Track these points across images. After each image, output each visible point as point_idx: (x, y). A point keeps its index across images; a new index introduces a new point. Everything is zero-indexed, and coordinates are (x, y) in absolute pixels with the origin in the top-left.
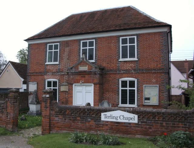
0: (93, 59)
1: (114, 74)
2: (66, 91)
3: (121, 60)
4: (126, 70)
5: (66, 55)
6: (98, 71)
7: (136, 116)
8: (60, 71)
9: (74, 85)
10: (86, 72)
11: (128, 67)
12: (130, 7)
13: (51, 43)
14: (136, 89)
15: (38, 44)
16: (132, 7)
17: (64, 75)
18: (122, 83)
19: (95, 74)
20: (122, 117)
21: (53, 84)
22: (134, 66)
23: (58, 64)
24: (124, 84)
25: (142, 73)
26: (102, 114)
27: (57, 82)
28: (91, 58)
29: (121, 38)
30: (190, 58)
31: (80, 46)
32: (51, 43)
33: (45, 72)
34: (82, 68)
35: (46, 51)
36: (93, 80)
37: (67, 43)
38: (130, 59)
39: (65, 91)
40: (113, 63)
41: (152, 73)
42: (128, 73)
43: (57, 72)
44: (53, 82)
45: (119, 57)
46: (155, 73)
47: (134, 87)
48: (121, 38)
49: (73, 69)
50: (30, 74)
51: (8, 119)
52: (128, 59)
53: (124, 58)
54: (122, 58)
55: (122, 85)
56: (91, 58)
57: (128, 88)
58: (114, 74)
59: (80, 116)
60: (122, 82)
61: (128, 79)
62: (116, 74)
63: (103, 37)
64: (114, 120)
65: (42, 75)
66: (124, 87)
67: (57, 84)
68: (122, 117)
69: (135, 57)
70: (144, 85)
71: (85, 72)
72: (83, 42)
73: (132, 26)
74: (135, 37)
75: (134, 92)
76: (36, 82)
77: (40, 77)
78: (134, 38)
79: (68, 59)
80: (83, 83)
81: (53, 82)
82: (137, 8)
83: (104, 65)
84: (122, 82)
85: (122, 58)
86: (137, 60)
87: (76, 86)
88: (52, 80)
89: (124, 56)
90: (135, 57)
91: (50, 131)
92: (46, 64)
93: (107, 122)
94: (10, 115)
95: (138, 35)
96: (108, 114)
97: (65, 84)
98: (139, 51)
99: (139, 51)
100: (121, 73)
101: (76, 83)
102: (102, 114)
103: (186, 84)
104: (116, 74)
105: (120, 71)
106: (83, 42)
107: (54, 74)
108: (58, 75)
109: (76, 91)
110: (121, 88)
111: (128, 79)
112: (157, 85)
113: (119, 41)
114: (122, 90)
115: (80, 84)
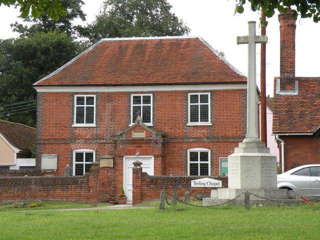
0: (150, 122)
1: (180, 143)
2: (109, 167)
3: (190, 124)
4: (197, 138)
5: (107, 114)
6: (161, 140)
7: (221, 182)
8: (98, 137)
9: (124, 158)
10: (143, 140)
11: (199, 133)
12: (200, 41)
13: (82, 93)
14: (209, 162)
15: (57, 93)
16: (203, 39)
17: (105, 143)
18: (191, 155)
19: (157, 143)
20: (209, 183)
21: (86, 156)
22: (207, 133)
23: (95, 127)
24: (194, 156)
25: (217, 142)
26: (192, 181)
27: (92, 154)
28: (146, 119)
29: (189, 94)
30: (318, 76)
31: (130, 102)
32: (82, 93)
33: (74, 138)
34: (137, 135)
35: (73, 106)
36: (153, 151)
37: (109, 97)
38: (202, 123)
39: (106, 167)
40: (179, 128)
41: (230, 142)
42: (199, 142)
43: (94, 139)
44: (86, 154)
45: (187, 120)
46: (235, 142)
47: (207, 160)
48: (189, 94)
49: (124, 136)
50: (42, 142)
51: (91, 194)
52: (199, 123)
53: (193, 121)
54: (191, 121)
55: (191, 158)
56: (146, 119)
57: (199, 162)
58: (180, 143)
59: (171, 185)
60: (191, 153)
61: (199, 150)
62: (183, 142)
63: (165, 92)
64: (203, 186)
65: (66, 143)
66: (193, 161)
67: (92, 156)
68: (209, 183)
69: (208, 121)
70: (220, 158)
71: (141, 140)
72: (134, 97)
73: (205, 78)
74: (209, 94)
75: (208, 167)
76: (55, 153)
77: (63, 146)
78: (207, 96)
79: (111, 120)
80: (140, 155)
81: (86, 154)
82: (210, 44)
83: (167, 130)
84: (191, 153)
85: (191, 121)
86: (211, 125)
87: (127, 160)
88: (85, 151)
89: (194, 119)
90: (208, 121)
91: (142, 200)
92: (73, 126)
93: (196, 188)
94: (93, 189)
95: (212, 92)
96: (197, 181)
97: (107, 157)
98: (214, 112)
99: (214, 112)
100: (190, 142)
101: (127, 155)
102: (192, 181)
103: (112, 161)
104: (183, 142)
105: (188, 138)
106: (134, 97)
107: (87, 142)
108: (95, 143)
109: (128, 166)
110: (189, 162)
111: (199, 150)
112: (151, 157)
113: (187, 98)
114: (191, 164)
115: (135, 157)
